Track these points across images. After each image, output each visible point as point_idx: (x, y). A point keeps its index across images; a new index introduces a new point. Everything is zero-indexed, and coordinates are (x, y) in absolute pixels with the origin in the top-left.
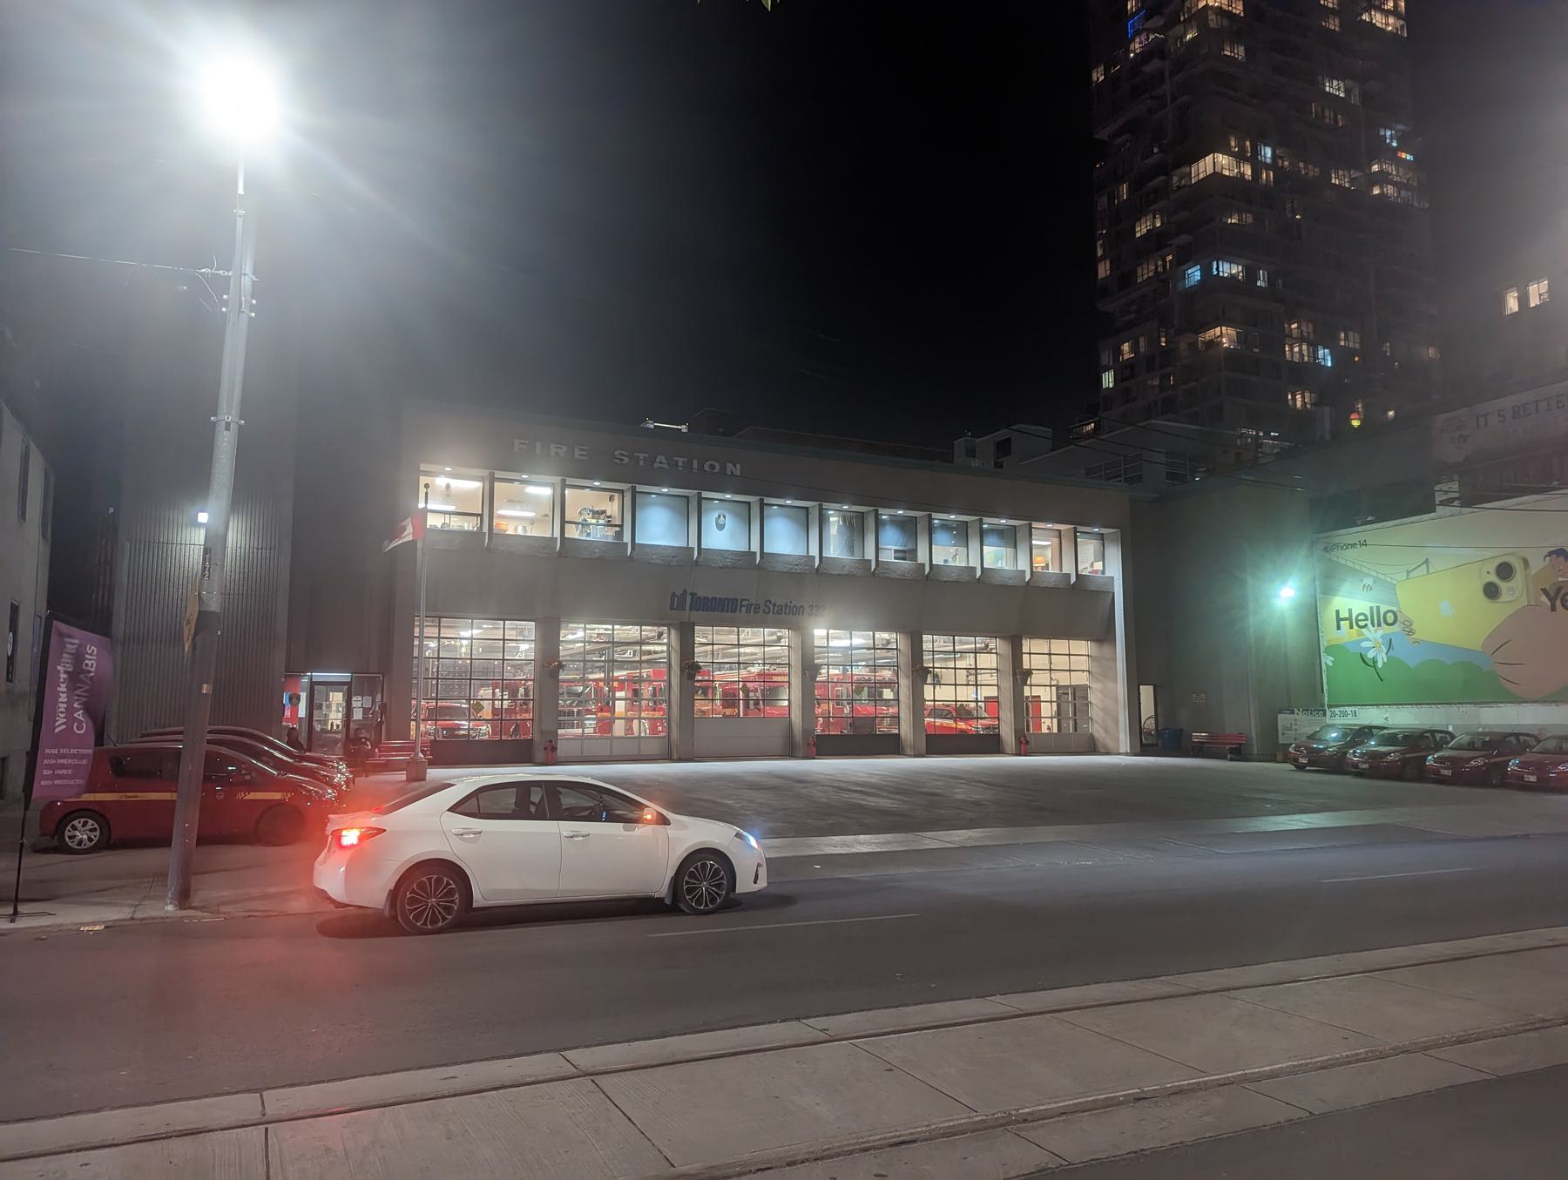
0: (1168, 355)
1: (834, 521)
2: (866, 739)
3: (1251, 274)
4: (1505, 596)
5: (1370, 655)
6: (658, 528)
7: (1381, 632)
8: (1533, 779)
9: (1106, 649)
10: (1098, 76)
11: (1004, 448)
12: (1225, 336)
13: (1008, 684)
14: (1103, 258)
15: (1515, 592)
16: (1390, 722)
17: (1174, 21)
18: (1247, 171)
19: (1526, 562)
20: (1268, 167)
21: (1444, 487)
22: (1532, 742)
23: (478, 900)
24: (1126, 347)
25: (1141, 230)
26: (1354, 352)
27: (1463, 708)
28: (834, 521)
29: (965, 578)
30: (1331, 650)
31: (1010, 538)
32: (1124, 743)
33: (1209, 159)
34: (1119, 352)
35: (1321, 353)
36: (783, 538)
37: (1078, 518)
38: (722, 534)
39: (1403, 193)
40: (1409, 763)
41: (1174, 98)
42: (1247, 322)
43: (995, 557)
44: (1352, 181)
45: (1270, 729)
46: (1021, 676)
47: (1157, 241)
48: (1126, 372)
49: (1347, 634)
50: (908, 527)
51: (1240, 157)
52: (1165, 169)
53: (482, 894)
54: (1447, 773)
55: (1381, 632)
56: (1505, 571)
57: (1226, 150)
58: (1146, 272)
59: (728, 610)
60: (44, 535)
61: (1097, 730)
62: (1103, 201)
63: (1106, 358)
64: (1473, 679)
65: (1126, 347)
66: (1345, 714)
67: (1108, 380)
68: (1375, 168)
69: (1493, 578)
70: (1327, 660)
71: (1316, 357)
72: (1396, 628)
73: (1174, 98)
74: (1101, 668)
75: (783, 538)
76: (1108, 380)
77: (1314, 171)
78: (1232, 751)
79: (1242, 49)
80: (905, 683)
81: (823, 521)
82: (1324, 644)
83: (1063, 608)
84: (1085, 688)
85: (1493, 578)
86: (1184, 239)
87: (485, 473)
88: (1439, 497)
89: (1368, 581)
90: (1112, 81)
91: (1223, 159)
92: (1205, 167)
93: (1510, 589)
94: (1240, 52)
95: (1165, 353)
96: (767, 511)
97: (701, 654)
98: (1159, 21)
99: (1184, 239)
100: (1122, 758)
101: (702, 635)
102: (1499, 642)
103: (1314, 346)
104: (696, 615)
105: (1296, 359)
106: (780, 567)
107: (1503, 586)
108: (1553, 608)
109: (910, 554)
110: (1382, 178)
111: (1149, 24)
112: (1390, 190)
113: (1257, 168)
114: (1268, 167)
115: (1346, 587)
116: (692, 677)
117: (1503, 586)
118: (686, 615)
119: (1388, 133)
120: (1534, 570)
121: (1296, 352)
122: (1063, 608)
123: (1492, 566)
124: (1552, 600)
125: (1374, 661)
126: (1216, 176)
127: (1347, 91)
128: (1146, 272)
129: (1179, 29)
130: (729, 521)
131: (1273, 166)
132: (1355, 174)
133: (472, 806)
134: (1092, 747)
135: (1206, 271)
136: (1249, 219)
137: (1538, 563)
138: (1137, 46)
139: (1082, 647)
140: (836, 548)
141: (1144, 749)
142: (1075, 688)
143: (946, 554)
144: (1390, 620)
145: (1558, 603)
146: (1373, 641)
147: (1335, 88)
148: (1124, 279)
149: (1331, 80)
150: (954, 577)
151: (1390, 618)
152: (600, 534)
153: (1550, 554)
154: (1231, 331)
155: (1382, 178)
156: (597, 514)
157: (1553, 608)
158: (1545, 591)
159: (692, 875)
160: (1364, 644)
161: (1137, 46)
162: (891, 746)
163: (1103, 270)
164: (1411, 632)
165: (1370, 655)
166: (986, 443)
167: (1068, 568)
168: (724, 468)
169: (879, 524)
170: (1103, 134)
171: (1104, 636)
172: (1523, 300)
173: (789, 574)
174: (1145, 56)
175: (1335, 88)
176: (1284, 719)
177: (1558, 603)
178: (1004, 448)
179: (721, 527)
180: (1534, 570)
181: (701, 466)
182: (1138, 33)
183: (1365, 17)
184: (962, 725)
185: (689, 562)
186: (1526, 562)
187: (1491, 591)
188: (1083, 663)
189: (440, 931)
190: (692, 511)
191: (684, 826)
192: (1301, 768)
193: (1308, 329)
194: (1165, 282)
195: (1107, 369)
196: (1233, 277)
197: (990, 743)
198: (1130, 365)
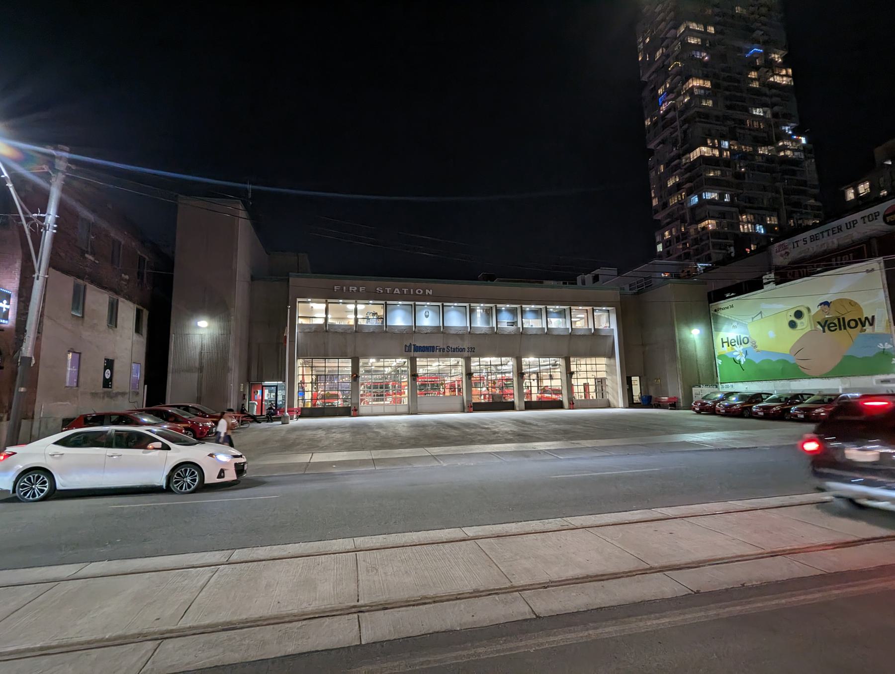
0: (685, 235)
1: (479, 312)
2: (498, 404)
3: (722, 196)
4: (799, 327)
5: (738, 358)
6: (399, 319)
7: (742, 347)
8: (802, 416)
9: (612, 361)
10: (648, 123)
11: (596, 279)
12: (711, 224)
13: (564, 378)
14: (655, 197)
15: (804, 325)
16: (749, 390)
17: (679, 94)
18: (717, 153)
19: (809, 309)
20: (726, 150)
21: (767, 276)
22: (833, 398)
23: (59, 486)
24: (667, 233)
25: (670, 183)
26: (774, 226)
27: (782, 382)
28: (479, 312)
29: (539, 332)
30: (720, 357)
31: (561, 314)
32: (621, 404)
33: (698, 150)
34: (663, 236)
35: (758, 228)
36: (455, 319)
37: (594, 303)
38: (427, 319)
39: (796, 154)
40: (746, 410)
41: (681, 127)
42: (720, 217)
43: (555, 323)
44: (769, 151)
45: (689, 396)
46: (570, 374)
47: (678, 187)
48: (667, 244)
49: (726, 349)
50: (513, 312)
51: (713, 147)
52: (679, 157)
53: (62, 483)
54: (762, 414)
55: (742, 347)
56: (799, 314)
57: (706, 145)
58: (673, 201)
59: (429, 351)
60: (138, 330)
61: (610, 397)
62: (653, 174)
63: (658, 239)
64: (788, 370)
65: (667, 233)
66: (728, 387)
67: (660, 248)
68: (781, 144)
69: (794, 319)
70: (719, 362)
71: (755, 229)
72: (749, 345)
73: (681, 127)
74: (610, 370)
75: (455, 319)
76: (660, 248)
77: (749, 149)
78: (671, 405)
79: (711, 102)
80: (515, 379)
81: (472, 311)
82: (717, 354)
84: (605, 379)
85: (794, 319)
86: (688, 185)
87: (324, 300)
88: (765, 281)
89: (735, 324)
90: (655, 124)
91: (704, 149)
92: (695, 154)
93: (802, 323)
94: (710, 103)
95: (683, 234)
96: (417, 307)
97: (573, 368)
98: (672, 96)
99: (688, 185)
100: (620, 409)
101: (420, 362)
102: (798, 349)
103: (754, 224)
104: (416, 354)
105: (746, 231)
106: (452, 332)
107: (798, 321)
108: (824, 331)
109: (514, 323)
110: (784, 148)
111: (669, 97)
112: (788, 153)
113: (721, 150)
114: (726, 150)
115: (725, 327)
116: (470, 378)
117: (798, 321)
118: (412, 354)
119: (787, 128)
120: (813, 312)
121: (745, 228)
122: (590, 344)
123: (792, 312)
124: (823, 327)
125: (740, 361)
126: (702, 157)
127: (764, 112)
128: (673, 201)
129: (681, 98)
130: (431, 314)
131: (729, 149)
132: (770, 148)
133: (62, 442)
134: (609, 406)
135: (700, 197)
136: (719, 173)
137: (815, 309)
138: (664, 108)
139: (603, 361)
140: (479, 322)
141: (631, 404)
142: (602, 379)
143: (532, 323)
144: (746, 341)
145: (826, 328)
146: (738, 352)
147: (758, 112)
148: (665, 205)
149: (756, 108)
150: (534, 332)
151: (746, 341)
152: (374, 322)
153: (821, 304)
154: (713, 222)
155: (784, 148)
156: (374, 314)
157: (824, 331)
158: (819, 323)
159: (179, 475)
160: (735, 354)
161: (664, 108)
162: (511, 406)
163: (655, 202)
164: (755, 347)
165: (738, 358)
166: (589, 277)
167: (591, 326)
168: (425, 292)
169: (498, 311)
170: (651, 146)
171: (611, 355)
172: (857, 193)
173: (457, 335)
174: (667, 112)
175: (758, 112)
176: (695, 390)
177: (826, 328)
178: (596, 279)
179: (427, 316)
180: (813, 312)
181: (414, 291)
182: (664, 102)
183: (772, 79)
184: (554, 396)
185: (413, 331)
186: (809, 309)
187: (792, 325)
188: (604, 368)
189: (193, 492)
190: (442, 313)
191: (178, 451)
192: (698, 413)
193: (751, 217)
194: (682, 204)
195: (659, 243)
196: (713, 199)
197: (559, 405)
198: (669, 240)
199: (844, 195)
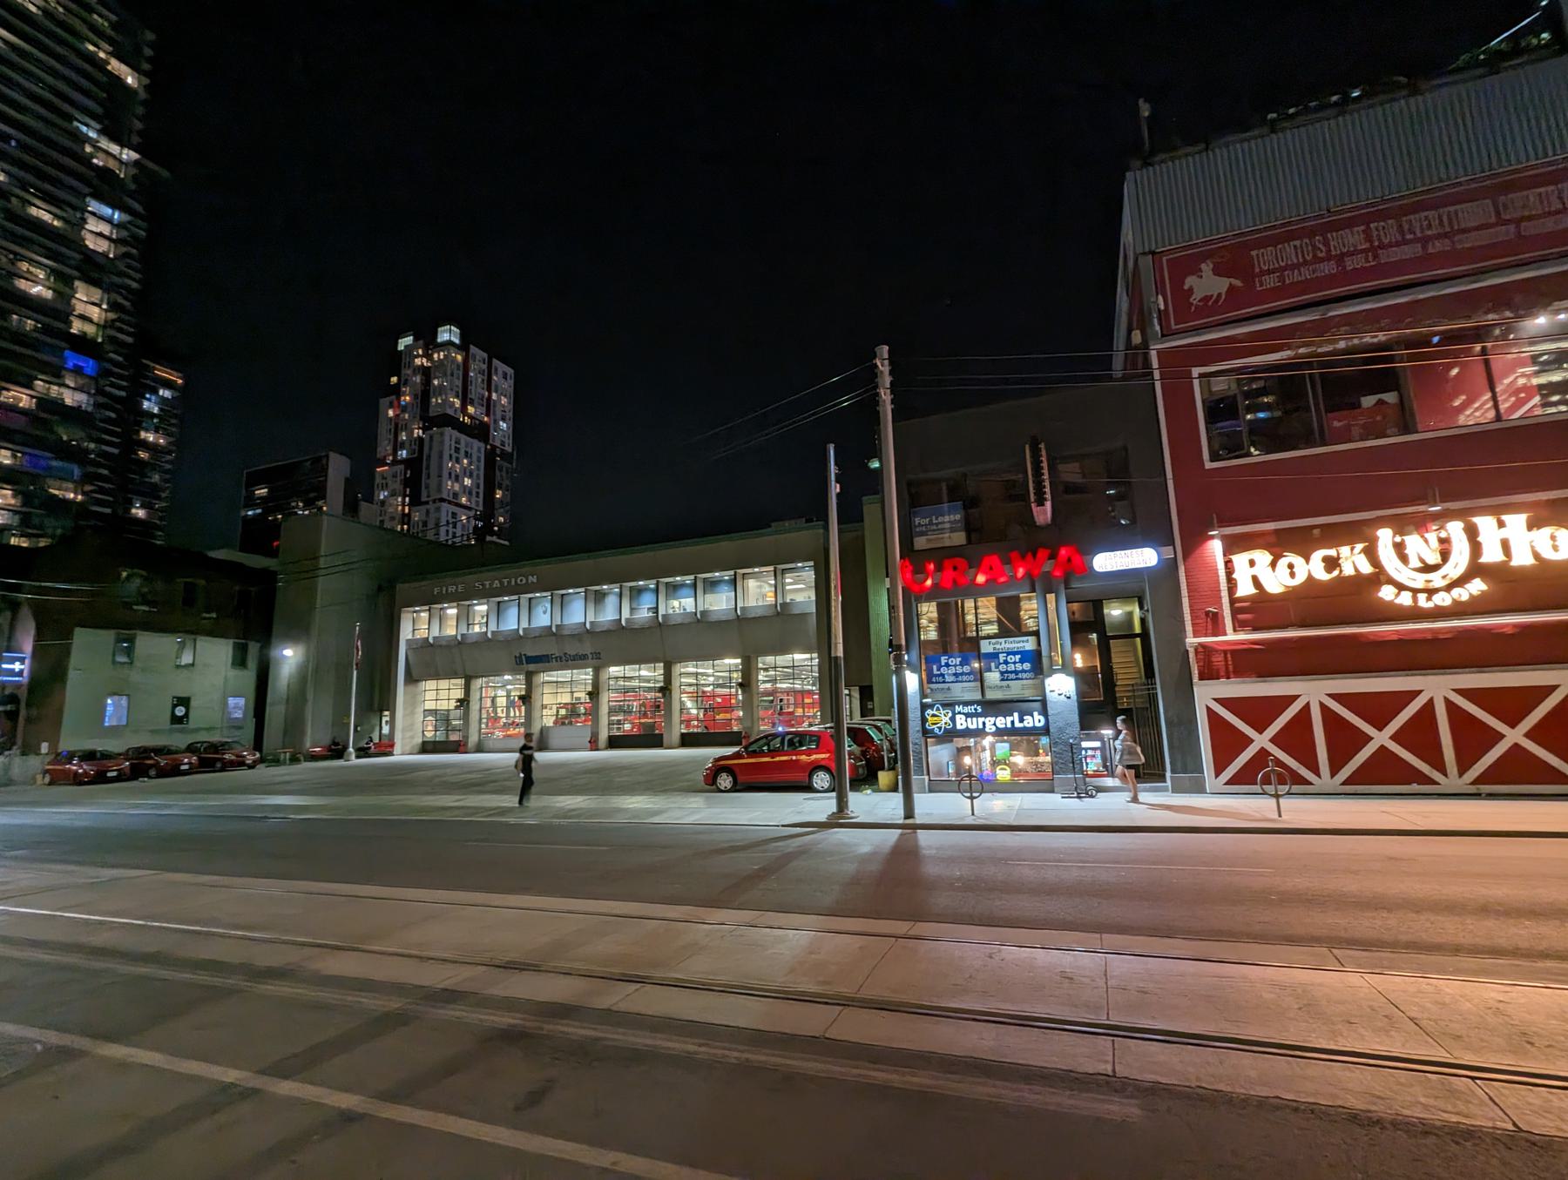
36: (578, 613)
37: (780, 560)
75: (578, 613)
83: (777, 629)
199: (402, 334)
